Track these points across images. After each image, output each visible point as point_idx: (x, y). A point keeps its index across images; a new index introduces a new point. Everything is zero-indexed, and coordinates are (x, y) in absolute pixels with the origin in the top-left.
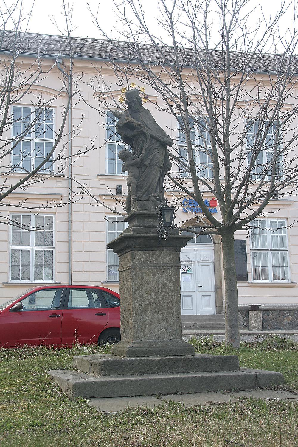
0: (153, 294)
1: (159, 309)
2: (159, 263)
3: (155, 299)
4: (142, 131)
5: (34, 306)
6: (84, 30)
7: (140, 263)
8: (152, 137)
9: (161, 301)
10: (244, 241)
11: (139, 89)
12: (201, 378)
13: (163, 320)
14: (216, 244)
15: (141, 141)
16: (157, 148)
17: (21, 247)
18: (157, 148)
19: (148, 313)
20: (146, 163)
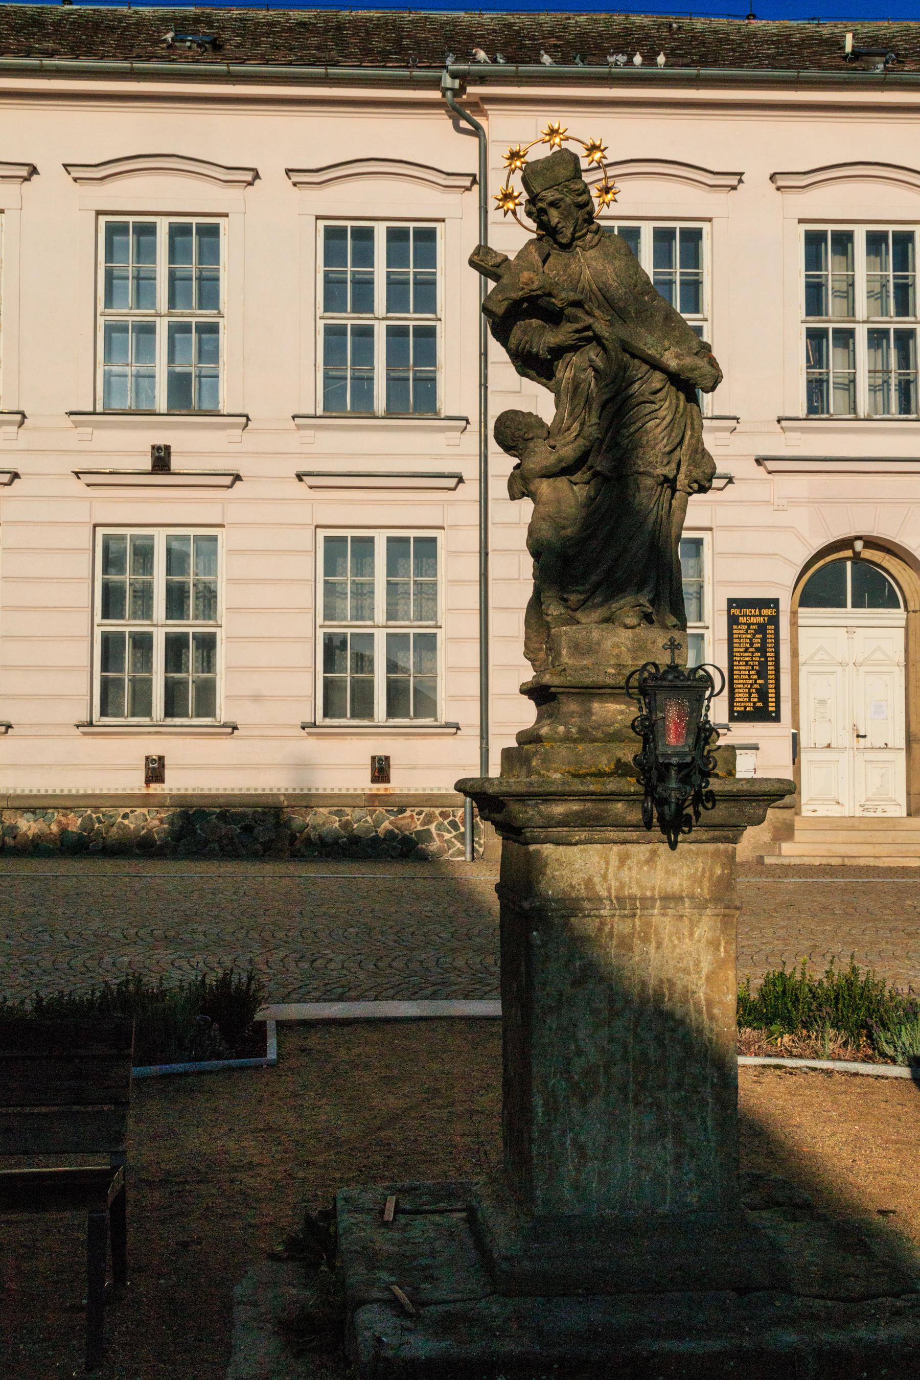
0: (618, 1023)
1: (642, 1085)
3: (625, 1045)
5: (386, 789)
9: (653, 1053)
11: (579, 150)
13: (660, 1133)
14: (914, 611)
17: (347, 628)
19: (596, 1103)
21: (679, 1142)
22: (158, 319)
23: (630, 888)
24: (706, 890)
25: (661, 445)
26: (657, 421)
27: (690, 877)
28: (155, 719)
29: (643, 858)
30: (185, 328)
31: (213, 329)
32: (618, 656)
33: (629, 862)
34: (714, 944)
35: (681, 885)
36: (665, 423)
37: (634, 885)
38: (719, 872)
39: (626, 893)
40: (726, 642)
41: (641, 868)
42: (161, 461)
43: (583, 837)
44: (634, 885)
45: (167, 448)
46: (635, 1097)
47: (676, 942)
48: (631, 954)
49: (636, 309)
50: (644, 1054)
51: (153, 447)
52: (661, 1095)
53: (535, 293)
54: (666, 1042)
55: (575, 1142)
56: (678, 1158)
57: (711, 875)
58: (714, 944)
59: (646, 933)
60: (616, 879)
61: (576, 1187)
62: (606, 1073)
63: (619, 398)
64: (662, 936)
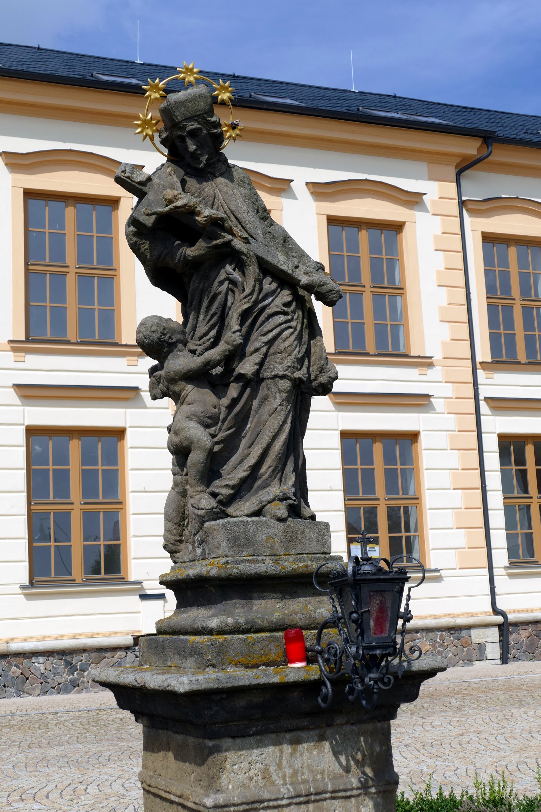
2: (319, 777)
4: (228, 243)
6: (309, 475)
7: (243, 785)
8: (267, 269)
10: (120, 573)
12: (360, 518)
15: (221, 283)
16: (286, 309)
18: (286, 309)
20: (247, 367)
32: (272, 548)
38: (378, 749)
39: (300, 779)
40: (309, 487)
41: (311, 753)
43: (259, 728)
44: (306, 771)
49: (262, 231)
53: (179, 210)
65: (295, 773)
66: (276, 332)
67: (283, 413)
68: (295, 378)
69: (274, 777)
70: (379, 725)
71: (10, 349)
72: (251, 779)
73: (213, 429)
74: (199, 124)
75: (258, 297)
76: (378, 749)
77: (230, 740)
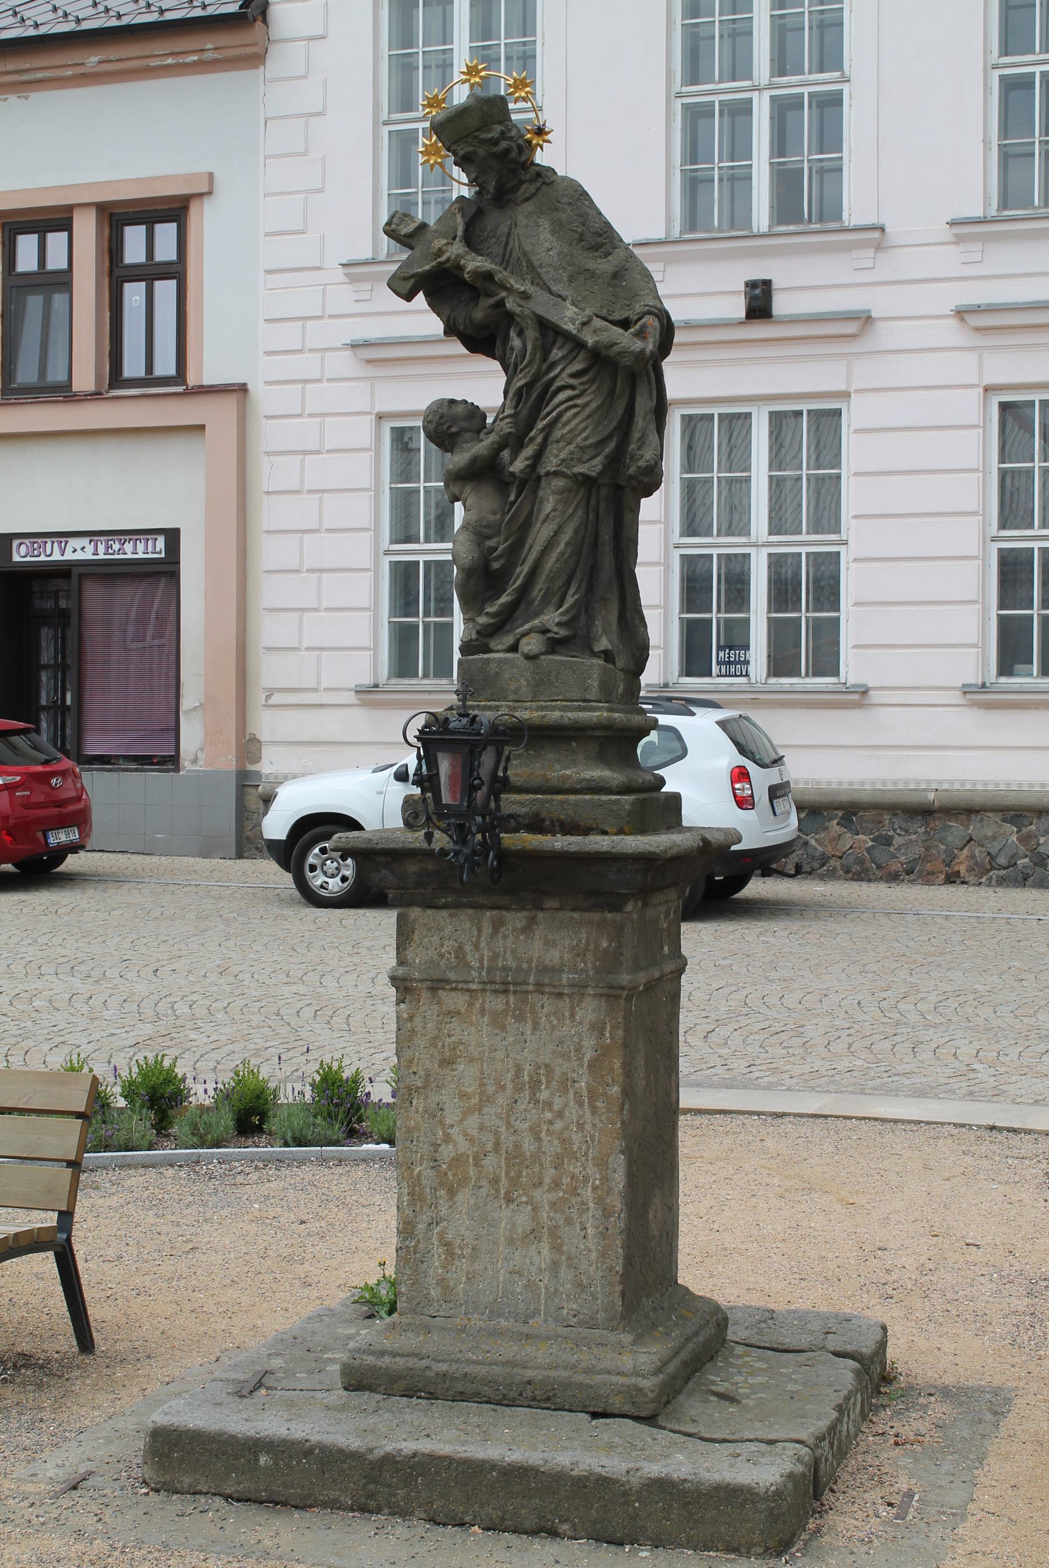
0: (490, 1110)
3: (497, 1134)
9: (528, 1146)
13: (534, 1234)
21: (557, 1248)
22: (755, 95)
23: (505, 959)
24: (590, 965)
25: (579, 439)
26: (575, 410)
27: (572, 949)
28: (753, 680)
29: (519, 926)
30: (794, 103)
31: (834, 101)
33: (503, 929)
34: (598, 1028)
35: (561, 958)
36: (587, 411)
37: (509, 955)
38: (605, 944)
39: (500, 964)
41: (517, 937)
42: (759, 303)
44: (509, 955)
45: (767, 284)
46: (507, 1193)
47: (555, 1022)
48: (504, 1034)
50: (517, 1146)
51: (747, 284)
52: (537, 1194)
54: (543, 1135)
55: (441, 1237)
56: (555, 1266)
57: (597, 948)
58: (598, 1028)
59: (521, 1011)
60: (489, 949)
61: (442, 1282)
62: (476, 1165)
63: (539, 384)
64: (540, 1015)
65: (495, 956)
66: (554, 414)
67: (557, 521)
68: (575, 475)
69: (469, 958)
70: (609, 916)
71: (952, 239)
72: (442, 956)
73: (495, 540)
74: (470, 145)
75: (540, 368)
76: (605, 944)
77: (419, 909)
